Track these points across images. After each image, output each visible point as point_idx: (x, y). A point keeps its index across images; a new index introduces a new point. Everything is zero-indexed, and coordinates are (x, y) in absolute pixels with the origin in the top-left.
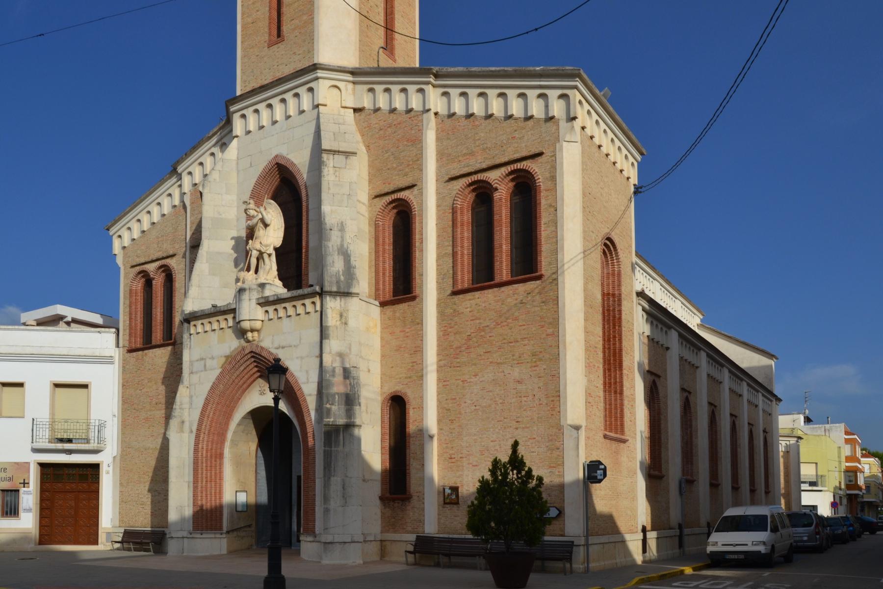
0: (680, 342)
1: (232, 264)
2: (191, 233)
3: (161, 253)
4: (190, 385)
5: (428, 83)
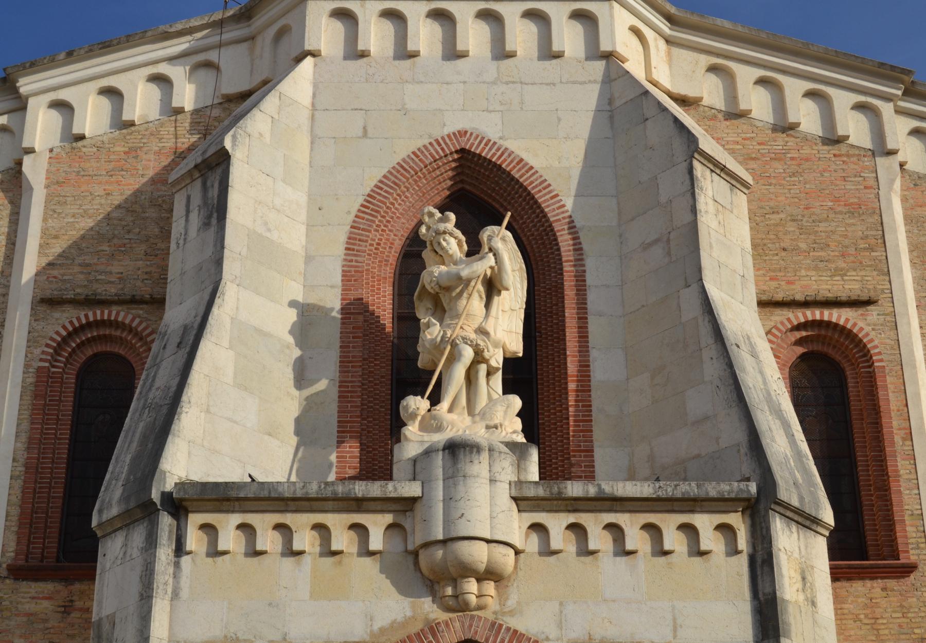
1: (288, 375)
5: (887, 98)
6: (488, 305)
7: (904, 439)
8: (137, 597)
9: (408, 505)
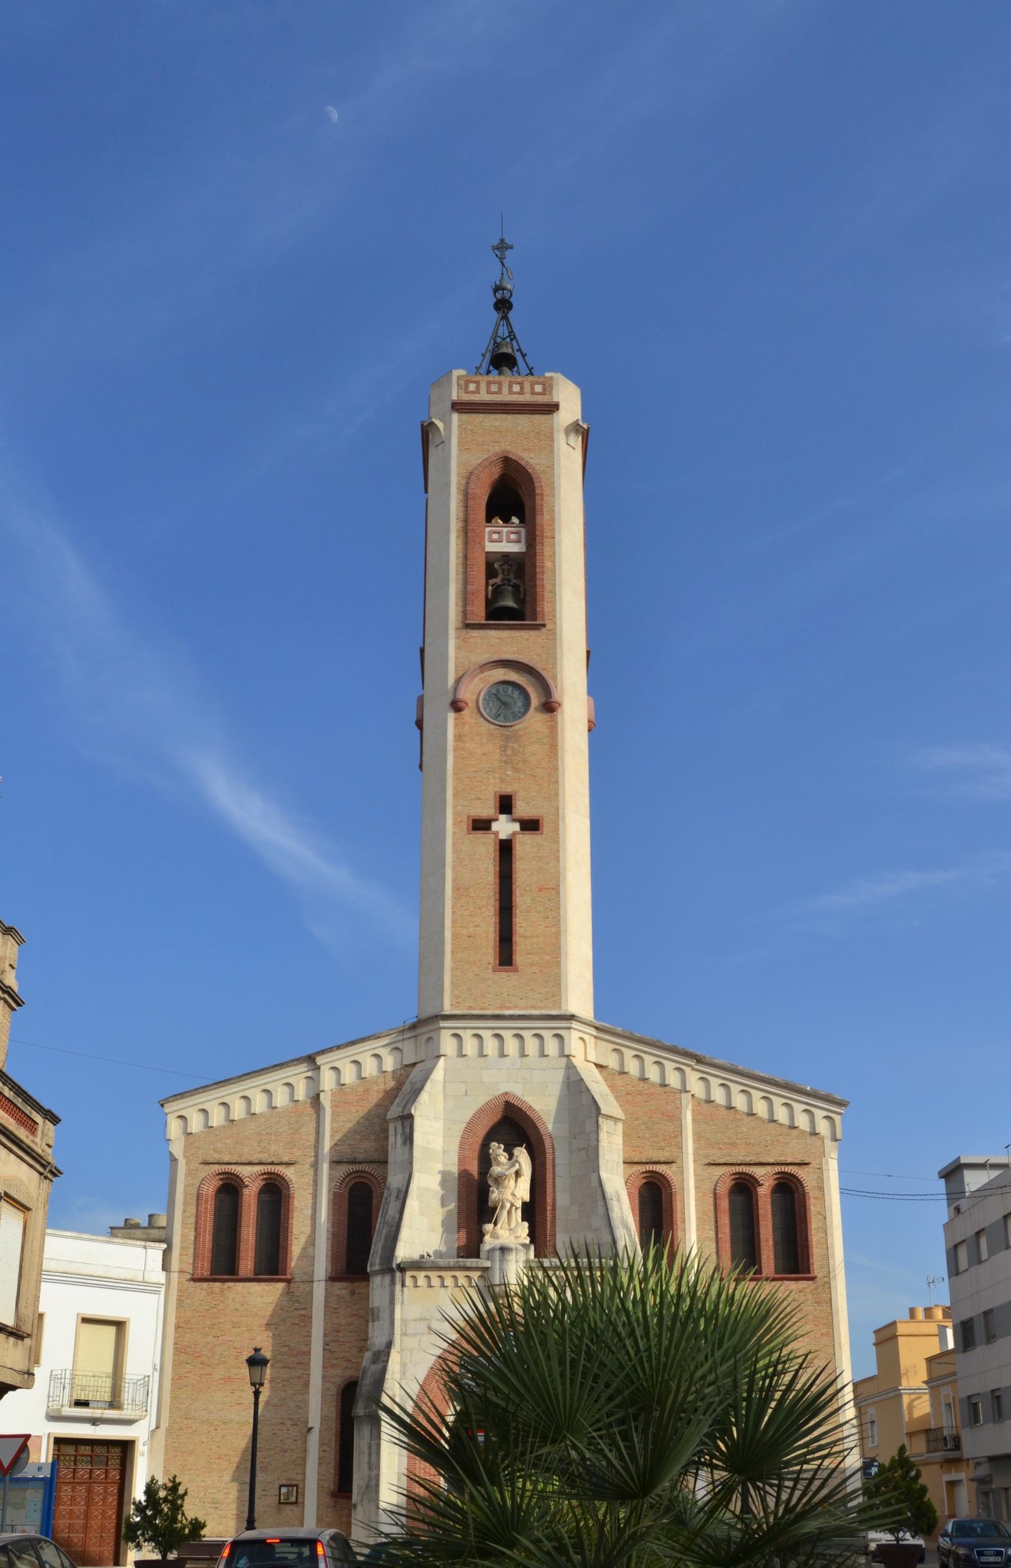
0: (49, 1176)
1: (439, 1203)
2: (333, 1143)
3: (265, 1155)
4: (401, 1350)
6: (516, 1181)
7: (682, 1223)
8: (388, 1303)
9: (486, 1269)
